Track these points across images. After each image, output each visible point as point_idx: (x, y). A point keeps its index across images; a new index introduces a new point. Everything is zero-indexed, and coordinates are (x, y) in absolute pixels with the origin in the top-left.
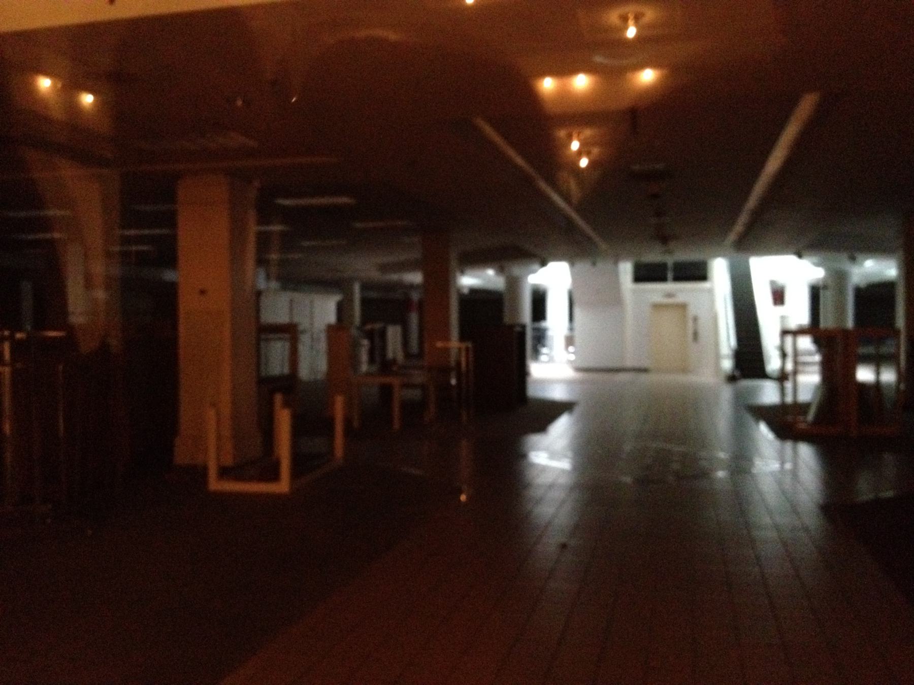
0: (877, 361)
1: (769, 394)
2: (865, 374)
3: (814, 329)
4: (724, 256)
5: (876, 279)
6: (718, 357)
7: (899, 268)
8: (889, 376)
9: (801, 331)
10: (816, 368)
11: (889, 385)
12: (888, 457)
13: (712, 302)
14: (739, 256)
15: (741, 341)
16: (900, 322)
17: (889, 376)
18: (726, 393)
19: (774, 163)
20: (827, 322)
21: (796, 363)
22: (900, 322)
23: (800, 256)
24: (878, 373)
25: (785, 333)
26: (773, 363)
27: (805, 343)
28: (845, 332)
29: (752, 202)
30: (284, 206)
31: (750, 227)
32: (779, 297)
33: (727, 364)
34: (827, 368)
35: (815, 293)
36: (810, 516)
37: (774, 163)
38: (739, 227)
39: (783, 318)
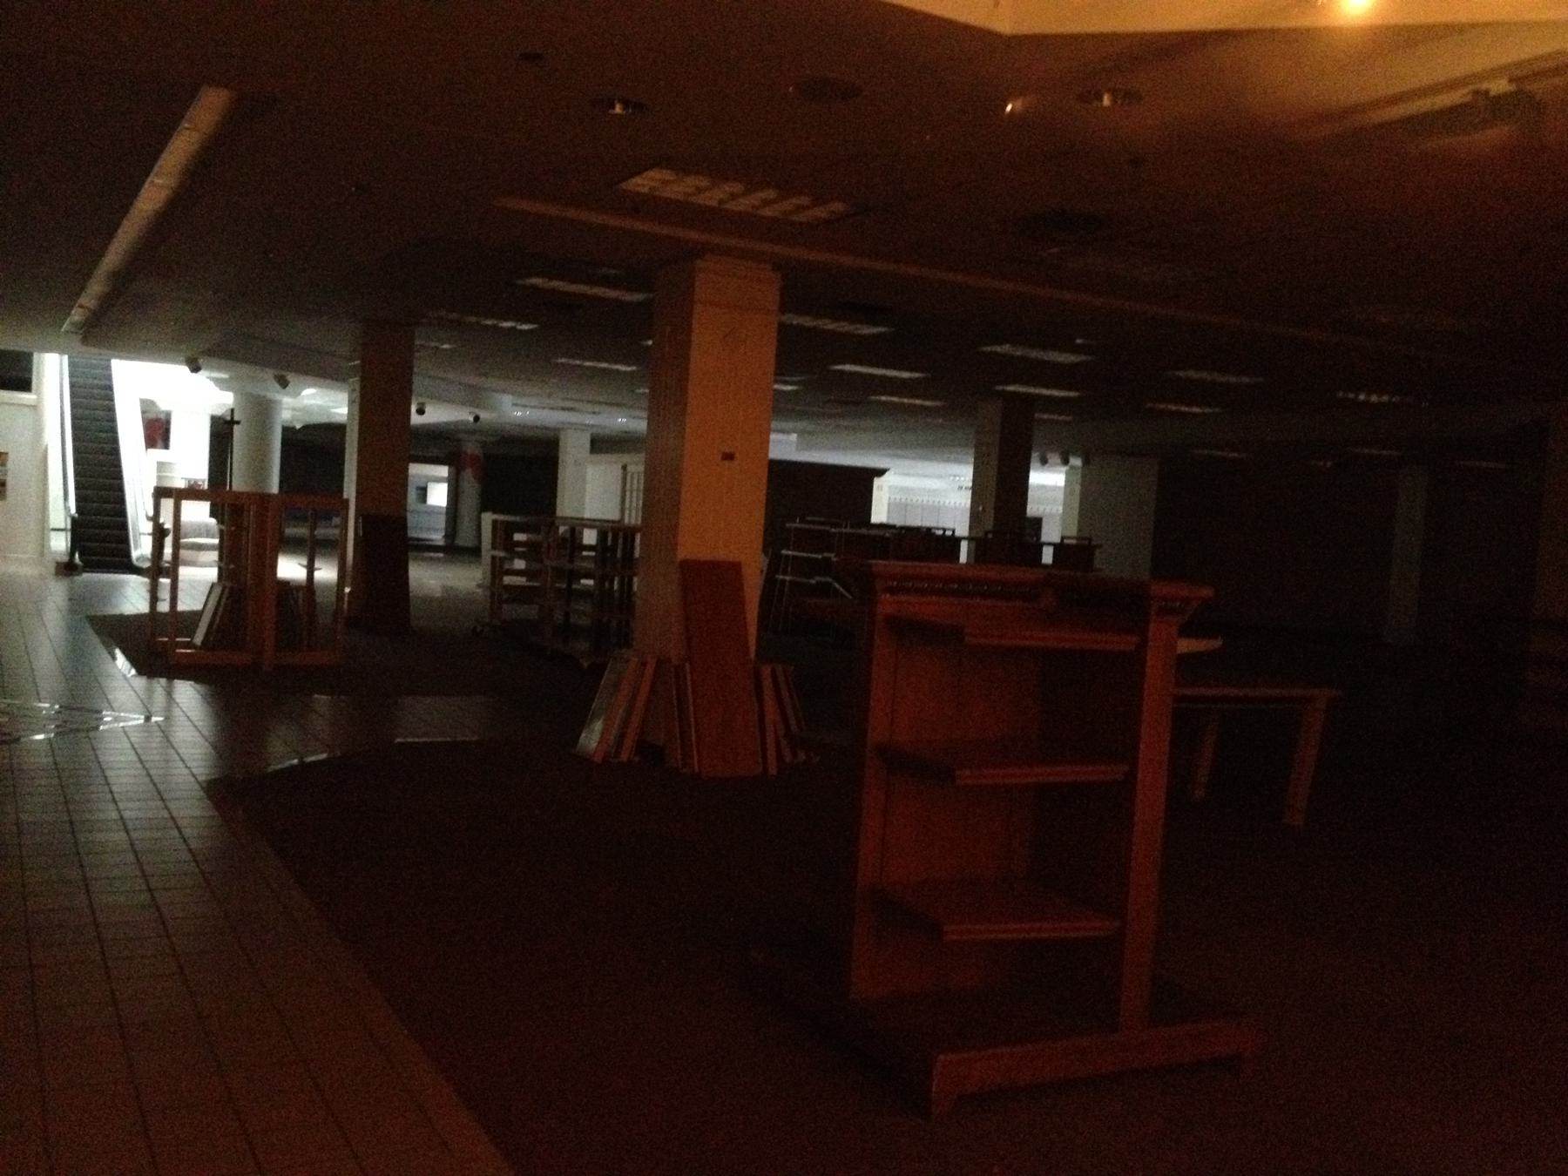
0: (311, 550)
1: (132, 597)
2: (290, 568)
3: (216, 491)
4: (62, 352)
5: (323, 419)
6: (44, 530)
7: (351, 403)
8: (326, 573)
9: (192, 493)
10: (213, 556)
11: (326, 586)
12: (322, 700)
13: (38, 432)
14: (92, 354)
15: (84, 555)
16: (350, 491)
17: (326, 573)
18: (56, 594)
19: (153, 194)
20: (239, 481)
21: (177, 546)
22: (350, 491)
23: (195, 369)
24: (311, 569)
25: (161, 493)
26: (141, 548)
27: (197, 513)
28: (263, 499)
29: (113, 257)
30: (698, 173)
31: (107, 303)
32: (158, 431)
33: (60, 543)
34: (231, 554)
35: (221, 431)
36: (191, 809)
37: (153, 194)
38: (90, 298)
39: (161, 466)
